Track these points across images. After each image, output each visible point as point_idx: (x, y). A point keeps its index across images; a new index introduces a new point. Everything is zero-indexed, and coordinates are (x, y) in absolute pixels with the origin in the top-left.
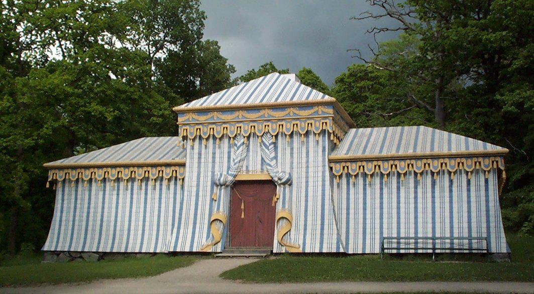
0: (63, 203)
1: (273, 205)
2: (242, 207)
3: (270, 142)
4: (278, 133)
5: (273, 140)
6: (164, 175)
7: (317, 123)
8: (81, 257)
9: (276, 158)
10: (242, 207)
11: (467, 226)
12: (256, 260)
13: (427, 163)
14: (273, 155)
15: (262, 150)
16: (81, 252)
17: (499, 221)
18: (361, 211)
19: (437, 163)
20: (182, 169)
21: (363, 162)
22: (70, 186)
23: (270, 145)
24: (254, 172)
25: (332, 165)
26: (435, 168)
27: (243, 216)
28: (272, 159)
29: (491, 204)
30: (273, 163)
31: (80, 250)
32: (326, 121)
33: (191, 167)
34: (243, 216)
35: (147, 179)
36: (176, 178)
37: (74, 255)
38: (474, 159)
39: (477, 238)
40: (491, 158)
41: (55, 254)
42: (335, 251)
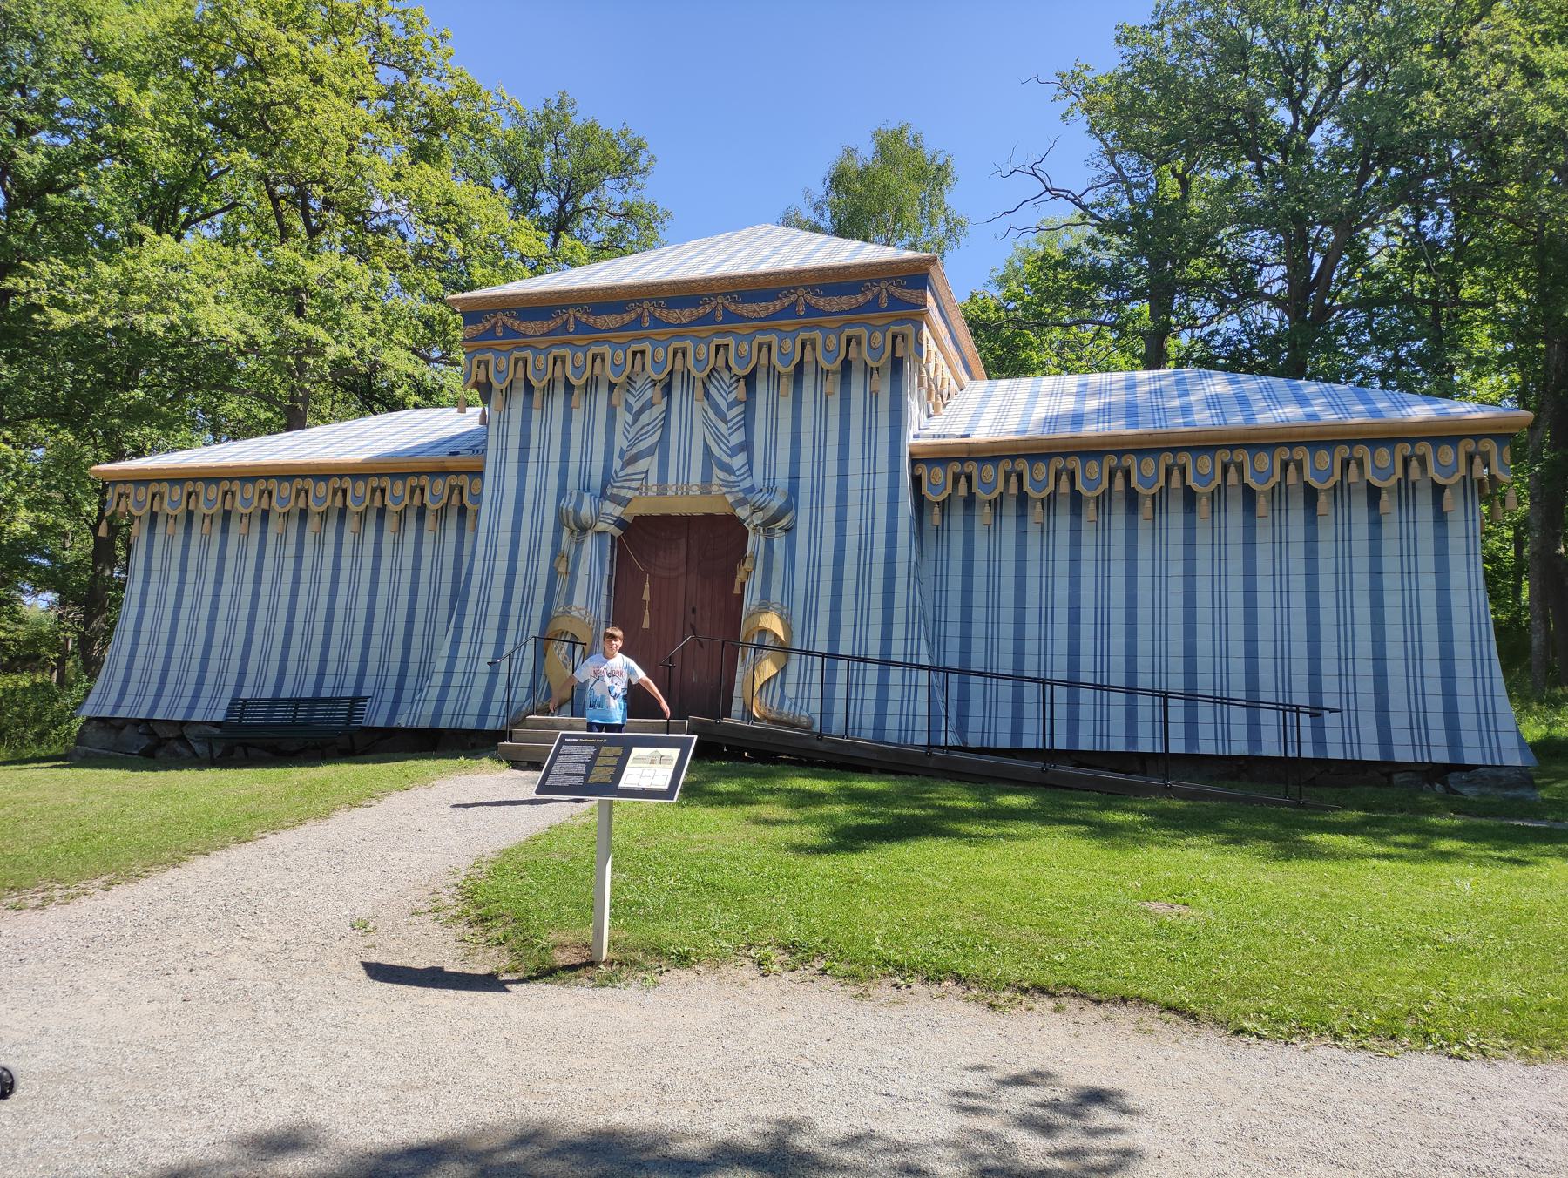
0: (146, 582)
1: (737, 591)
2: (646, 596)
3: (731, 397)
4: (754, 370)
5: (740, 392)
6: (349, 502)
7: (745, 345)
8: (182, 739)
9: (746, 447)
10: (646, 596)
11: (1370, 671)
12: (1330, 817)
13: (1065, 469)
14: (737, 438)
15: (706, 422)
16: (183, 723)
17: (1485, 656)
18: (151, 598)
19: (941, 474)
20: (478, 481)
21: (1236, 452)
22: (1102, 527)
23: (730, 406)
24: (682, 486)
25: (922, 470)
26: (1448, 471)
27: (646, 624)
28: (734, 452)
29: (1459, 600)
30: (739, 461)
31: (179, 716)
32: (642, 347)
33: (500, 477)
34: (646, 624)
35: (304, 514)
36: (970, 501)
37: (163, 732)
38: (1399, 447)
39: (1277, 707)
40: (1278, 450)
41: (113, 727)
42: (1182, 751)
